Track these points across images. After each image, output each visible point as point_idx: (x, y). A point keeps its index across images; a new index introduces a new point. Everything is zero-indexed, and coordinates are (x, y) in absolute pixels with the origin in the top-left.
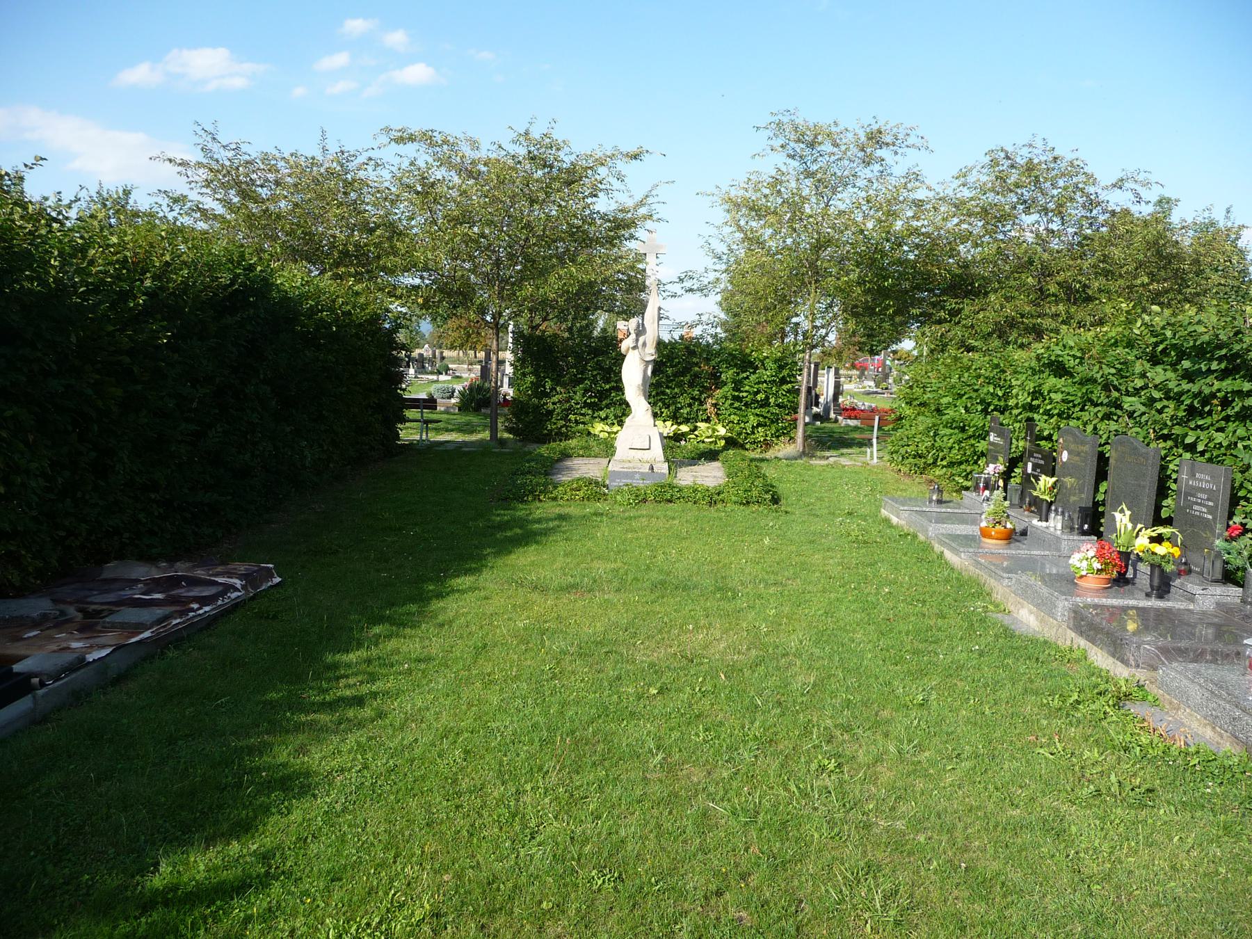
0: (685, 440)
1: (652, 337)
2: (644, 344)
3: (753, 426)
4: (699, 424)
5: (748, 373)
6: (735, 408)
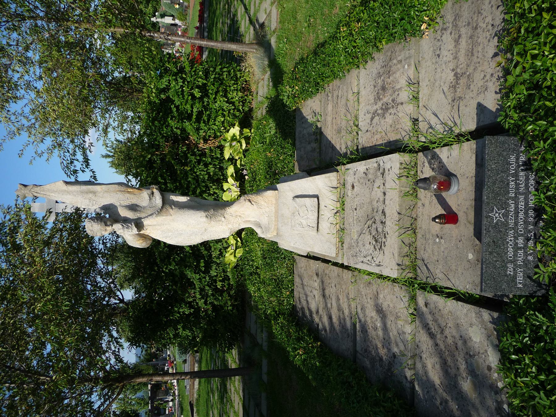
0: (243, 170)
1: (120, 196)
2: (133, 208)
3: (227, 102)
4: (227, 156)
5: (173, 106)
6: (209, 120)
